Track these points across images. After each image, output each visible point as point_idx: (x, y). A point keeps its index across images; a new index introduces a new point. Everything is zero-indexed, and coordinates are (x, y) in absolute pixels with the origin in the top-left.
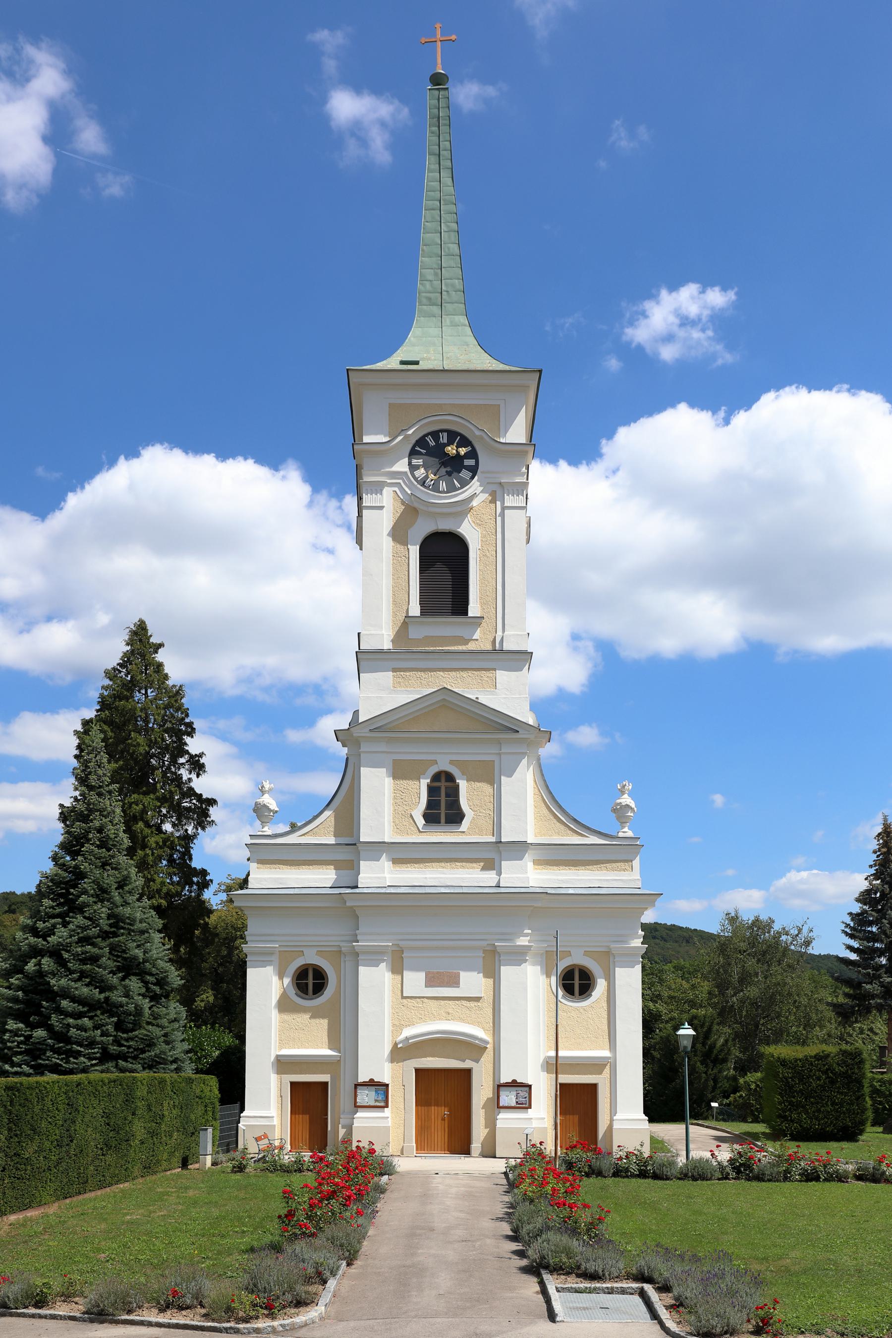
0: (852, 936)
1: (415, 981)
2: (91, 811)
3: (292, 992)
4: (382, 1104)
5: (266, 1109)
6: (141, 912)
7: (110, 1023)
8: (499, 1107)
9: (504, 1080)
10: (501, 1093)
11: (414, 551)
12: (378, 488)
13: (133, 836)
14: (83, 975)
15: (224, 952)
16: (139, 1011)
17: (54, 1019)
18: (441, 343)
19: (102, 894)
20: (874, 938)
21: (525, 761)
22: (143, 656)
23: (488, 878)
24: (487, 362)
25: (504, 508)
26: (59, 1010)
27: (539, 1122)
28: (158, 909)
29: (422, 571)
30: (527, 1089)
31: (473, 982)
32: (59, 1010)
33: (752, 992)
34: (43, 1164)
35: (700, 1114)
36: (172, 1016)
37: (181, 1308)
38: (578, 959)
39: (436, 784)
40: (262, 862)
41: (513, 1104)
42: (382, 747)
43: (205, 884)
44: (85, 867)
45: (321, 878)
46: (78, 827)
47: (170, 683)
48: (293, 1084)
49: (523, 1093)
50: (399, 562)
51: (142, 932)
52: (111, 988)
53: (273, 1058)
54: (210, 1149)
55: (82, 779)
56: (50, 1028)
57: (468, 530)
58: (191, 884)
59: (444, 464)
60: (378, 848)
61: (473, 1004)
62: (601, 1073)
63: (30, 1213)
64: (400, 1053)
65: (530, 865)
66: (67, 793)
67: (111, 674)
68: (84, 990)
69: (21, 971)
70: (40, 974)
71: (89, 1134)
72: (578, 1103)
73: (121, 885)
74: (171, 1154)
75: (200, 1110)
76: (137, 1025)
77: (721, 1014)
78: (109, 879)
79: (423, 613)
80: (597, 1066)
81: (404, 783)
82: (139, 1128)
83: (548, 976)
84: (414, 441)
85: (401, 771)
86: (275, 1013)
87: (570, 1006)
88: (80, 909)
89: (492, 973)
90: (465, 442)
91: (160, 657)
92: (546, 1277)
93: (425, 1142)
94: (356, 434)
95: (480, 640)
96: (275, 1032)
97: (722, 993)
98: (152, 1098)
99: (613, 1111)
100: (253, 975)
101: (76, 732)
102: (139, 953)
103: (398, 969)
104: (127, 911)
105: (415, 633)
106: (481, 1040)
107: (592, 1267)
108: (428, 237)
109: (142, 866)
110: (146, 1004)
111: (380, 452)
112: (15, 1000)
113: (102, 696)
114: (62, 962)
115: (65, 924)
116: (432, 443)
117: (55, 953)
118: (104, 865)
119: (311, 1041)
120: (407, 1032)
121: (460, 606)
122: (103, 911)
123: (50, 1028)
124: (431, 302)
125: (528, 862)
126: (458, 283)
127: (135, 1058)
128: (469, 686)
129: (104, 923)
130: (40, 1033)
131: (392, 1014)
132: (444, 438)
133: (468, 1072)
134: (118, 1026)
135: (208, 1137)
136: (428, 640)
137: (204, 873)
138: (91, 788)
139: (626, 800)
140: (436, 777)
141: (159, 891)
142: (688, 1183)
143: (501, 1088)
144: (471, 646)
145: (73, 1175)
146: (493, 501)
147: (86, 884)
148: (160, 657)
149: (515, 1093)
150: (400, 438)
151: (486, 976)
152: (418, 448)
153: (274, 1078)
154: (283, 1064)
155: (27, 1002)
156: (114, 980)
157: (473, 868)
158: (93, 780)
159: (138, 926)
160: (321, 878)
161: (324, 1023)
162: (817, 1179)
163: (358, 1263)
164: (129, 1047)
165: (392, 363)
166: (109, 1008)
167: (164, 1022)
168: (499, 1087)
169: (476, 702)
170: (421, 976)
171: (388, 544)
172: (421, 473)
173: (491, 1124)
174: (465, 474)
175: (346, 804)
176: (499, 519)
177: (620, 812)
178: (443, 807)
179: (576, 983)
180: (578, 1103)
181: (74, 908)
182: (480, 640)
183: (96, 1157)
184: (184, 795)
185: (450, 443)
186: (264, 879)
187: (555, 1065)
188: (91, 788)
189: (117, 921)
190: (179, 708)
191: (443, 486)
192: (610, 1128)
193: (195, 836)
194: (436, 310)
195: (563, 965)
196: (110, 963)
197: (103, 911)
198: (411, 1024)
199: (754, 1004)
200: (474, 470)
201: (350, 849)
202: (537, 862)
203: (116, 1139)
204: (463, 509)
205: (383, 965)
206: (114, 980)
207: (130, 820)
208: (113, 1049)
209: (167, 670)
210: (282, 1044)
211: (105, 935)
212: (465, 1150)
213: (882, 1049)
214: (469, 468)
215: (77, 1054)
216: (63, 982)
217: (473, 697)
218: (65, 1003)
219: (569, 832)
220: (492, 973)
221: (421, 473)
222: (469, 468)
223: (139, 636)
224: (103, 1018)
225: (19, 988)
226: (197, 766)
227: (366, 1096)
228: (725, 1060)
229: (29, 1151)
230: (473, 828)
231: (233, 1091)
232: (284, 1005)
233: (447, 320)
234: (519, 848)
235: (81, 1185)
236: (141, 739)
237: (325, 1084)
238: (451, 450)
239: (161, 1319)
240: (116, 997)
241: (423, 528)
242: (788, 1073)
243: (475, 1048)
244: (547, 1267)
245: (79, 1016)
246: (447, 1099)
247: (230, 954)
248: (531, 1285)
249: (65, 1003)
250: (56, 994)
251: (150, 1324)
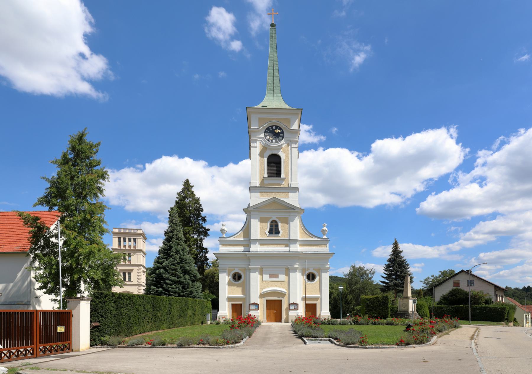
0: (386, 271)
1: (266, 277)
2: (174, 230)
3: (232, 280)
5: (225, 311)
6: (189, 257)
7: (180, 287)
11: (266, 160)
12: (255, 141)
13: (186, 238)
14: (172, 274)
15: (212, 280)
16: (189, 284)
17: (164, 286)
18: (273, 101)
19: (177, 252)
20: (392, 271)
21: (297, 218)
22: (188, 189)
23: (286, 249)
24: (287, 107)
25: (291, 148)
26: (166, 283)
27: (301, 312)
28: (194, 258)
29: (268, 165)
31: (282, 277)
32: (166, 283)
33: (358, 286)
34: (163, 319)
35: (344, 316)
36: (198, 286)
37: (203, 344)
38: (311, 271)
40: (223, 245)
43: (207, 252)
44: (172, 245)
45: (240, 249)
46: (170, 234)
47: (196, 197)
48: (232, 304)
49: (296, 306)
50: (262, 163)
51: (189, 263)
52: (181, 277)
54: (209, 319)
55: (171, 221)
56: (163, 288)
57: (281, 154)
58: (203, 252)
59: (274, 135)
60: (256, 241)
63: (159, 331)
64: (262, 296)
65: (298, 246)
66: (165, 226)
67: (179, 194)
68: (173, 278)
69: (155, 273)
70: (160, 274)
71: (175, 312)
72: (311, 308)
73: (183, 250)
74: (199, 320)
75: (206, 310)
76: (188, 288)
77: (350, 291)
78: (179, 248)
79: (268, 176)
80: (316, 299)
81: (263, 224)
82: (189, 312)
83: (303, 276)
85: (262, 220)
86: (227, 286)
87: (309, 283)
88: (171, 256)
89: (288, 275)
90: (280, 129)
91: (193, 189)
92: (303, 338)
93: (269, 319)
94: (249, 127)
95: (284, 184)
96: (227, 291)
97: (350, 287)
98: (193, 305)
99: (321, 310)
101: (169, 211)
102: (188, 268)
103: (261, 274)
104: (185, 257)
105: (266, 182)
107: (316, 335)
108: (270, 71)
109: (189, 246)
110: (191, 282)
111: (256, 131)
112: (153, 281)
113: (176, 201)
114: (166, 271)
115: (167, 260)
116: (271, 129)
117: (164, 268)
118: (178, 245)
119: (237, 293)
120: (264, 290)
121: (279, 174)
122: (178, 257)
123: (163, 288)
124: (271, 90)
125: (298, 245)
126: (278, 85)
127: (188, 296)
128: (281, 197)
129: (178, 260)
130: (161, 289)
131: (259, 285)
132: (274, 128)
133: (281, 301)
134: (183, 288)
135: (209, 316)
136: (270, 184)
137: (206, 249)
138: (173, 224)
139: (325, 228)
140: (272, 222)
141: (194, 253)
142: (341, 326)
144: (282, 186)
145: (171, 323)
146: (288, 146)
147: (173, 250)
148: (193, 189)
150: (193, 346)
151: (286, 275)
153: (227, 303)
154: (229, 299)
155: (156, 281)
156: (182, 275)
158: (174, 221)
159: (188, 261)
160: (240, 249)
161: (241, 288)
162: (376, 324)
163: (251, 338)
165: (260, 106)
166: (180, 283)
167: (196, 287)
168: (290, 304)
169: (283, 201)
170: (268, 276)
171: (258, 157)
172: (268, 137)
173: (287, 314)
174: (280, 138)
175: (246, 229)
177: (323, 232)
178: (274, 230)
179: (311, 277)
180: (311, 308)
181: (169, 256)
182: (284, 184)
183: (178, 319)
184: (200, 228)
185: (276, 129)
186: (224, 249)
187: (305, 299)
188: (173, 224)
189: (182, 260)
190: (199, 204)
191: (274, 141)
192: (320, 315)
193: (203, 239)
194: (272, 92)
195: (307, 272)
196: (180, 271)
197: (178, 257)
199: (359, 289)
200: (283, 137)
201: (248, 241)
202: (300, 245)
203: (183, 314)
204: (280, 148)
205: (257, 273)
206: (182, 275)
207: (185, 234)
208: (182, 294)
209: (195, 193)
210: (229, 294)
211: (179, 263)
212: (281, 321)
213: (393, 301)
214: (281, 136)
215: (171, 295)
216: (167, 275)
218: (167, 281)
220: (288, 275)
222: (281, 136)
223: (187, 183)
224: (179, 286)
225: (154, 278)
226: (204, 220)
227: (253, 307)
228: (351, 303)
229: (159, 314)
230: (283, 236)
231: (215, 305)
232: (230, 284)
233: (275, 95)
234: (295, 241)
235: (174, 326)
236: (188, 212)
237: (241, 304)
238: (276, 131)
239: (198, 346)
240: (182, 280)
241: (268, 153)
242: (368, 302)
243: (283, 294)
244: (303, 336)
245: (172, 285)
246: (275, 308)
247: (213, 280)
248: (300, 340)
249: (167, 281)
250: (165, 279)
251: (195, 347)
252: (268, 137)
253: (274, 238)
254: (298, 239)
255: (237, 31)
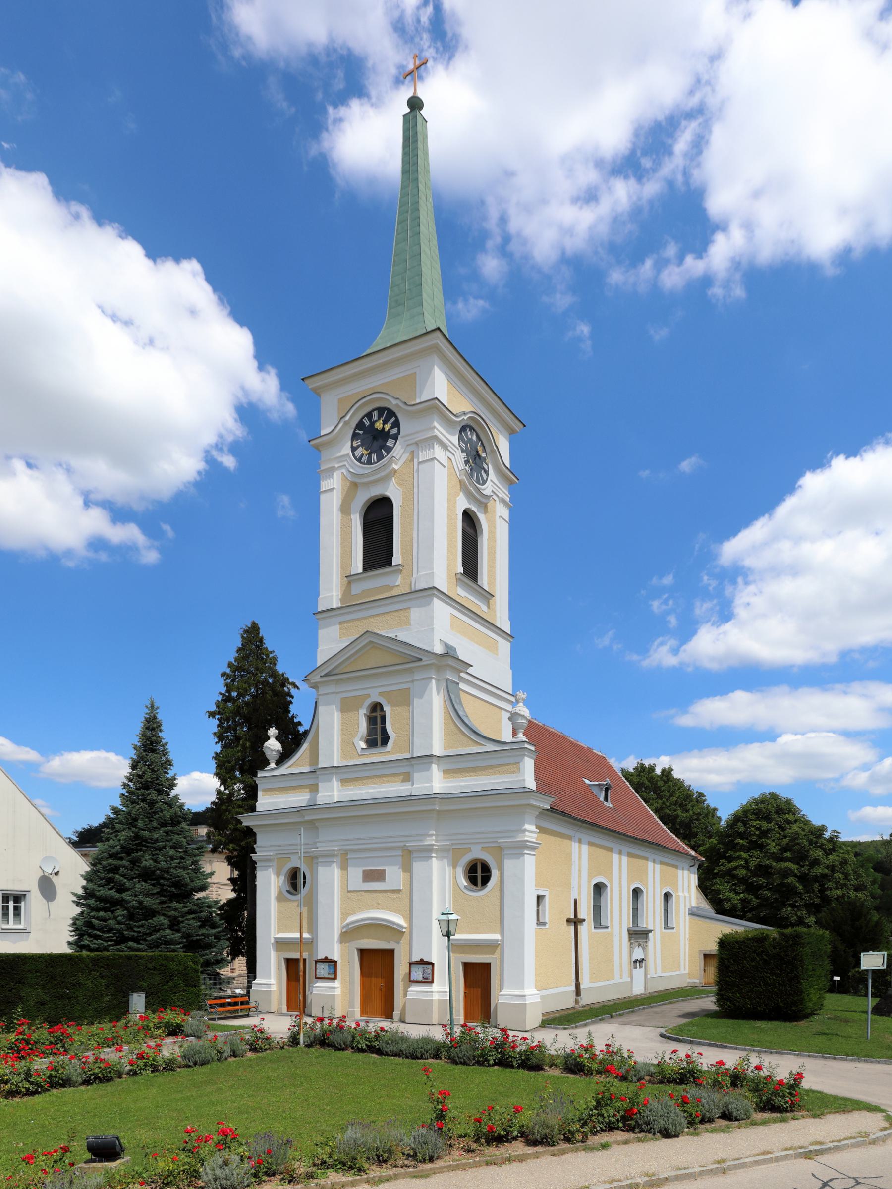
4: (333, 977)
8: (410, 981)
9: (414, 959)
10: (412, 969)
30: (430, 967)
31: (395, 876)
38: (477, 854)
39: (374, 714)
41: (421, 979)
42: (332, 689)
53: (272, 941)
61: (395, 895)
62: (493, 953)
64: (348, 934)
80: (491, 946)
83: (454, 867)
84: (354, 426)
100: (260, 875)
103: (344, 867)
105: (356, 589)
106: (398, 925)
120: (351, 919)
132: (365, 459)
133: (391, 952)
143: (413, 966)
149: (421, 970)
150: (340, 425)
152: (357, 431)
153: (273, 954)
154: (280, 944)
157: (395, 781)
164: (139, 932)
172: (358, 452)
174: (390, 443)
176: (416, 475)
187: (454, 947)
191: (374, 457)
198: (354, 913)
205: (270, 870)
217: (393, 636)
219: (470, 743)
220: (407, 868)
221: (360, 451)
227: (323, 970)
243: (395, 931)
252: (358, 452)
253: (378, 755)
254: (438, 749)
255: (266, 387)
